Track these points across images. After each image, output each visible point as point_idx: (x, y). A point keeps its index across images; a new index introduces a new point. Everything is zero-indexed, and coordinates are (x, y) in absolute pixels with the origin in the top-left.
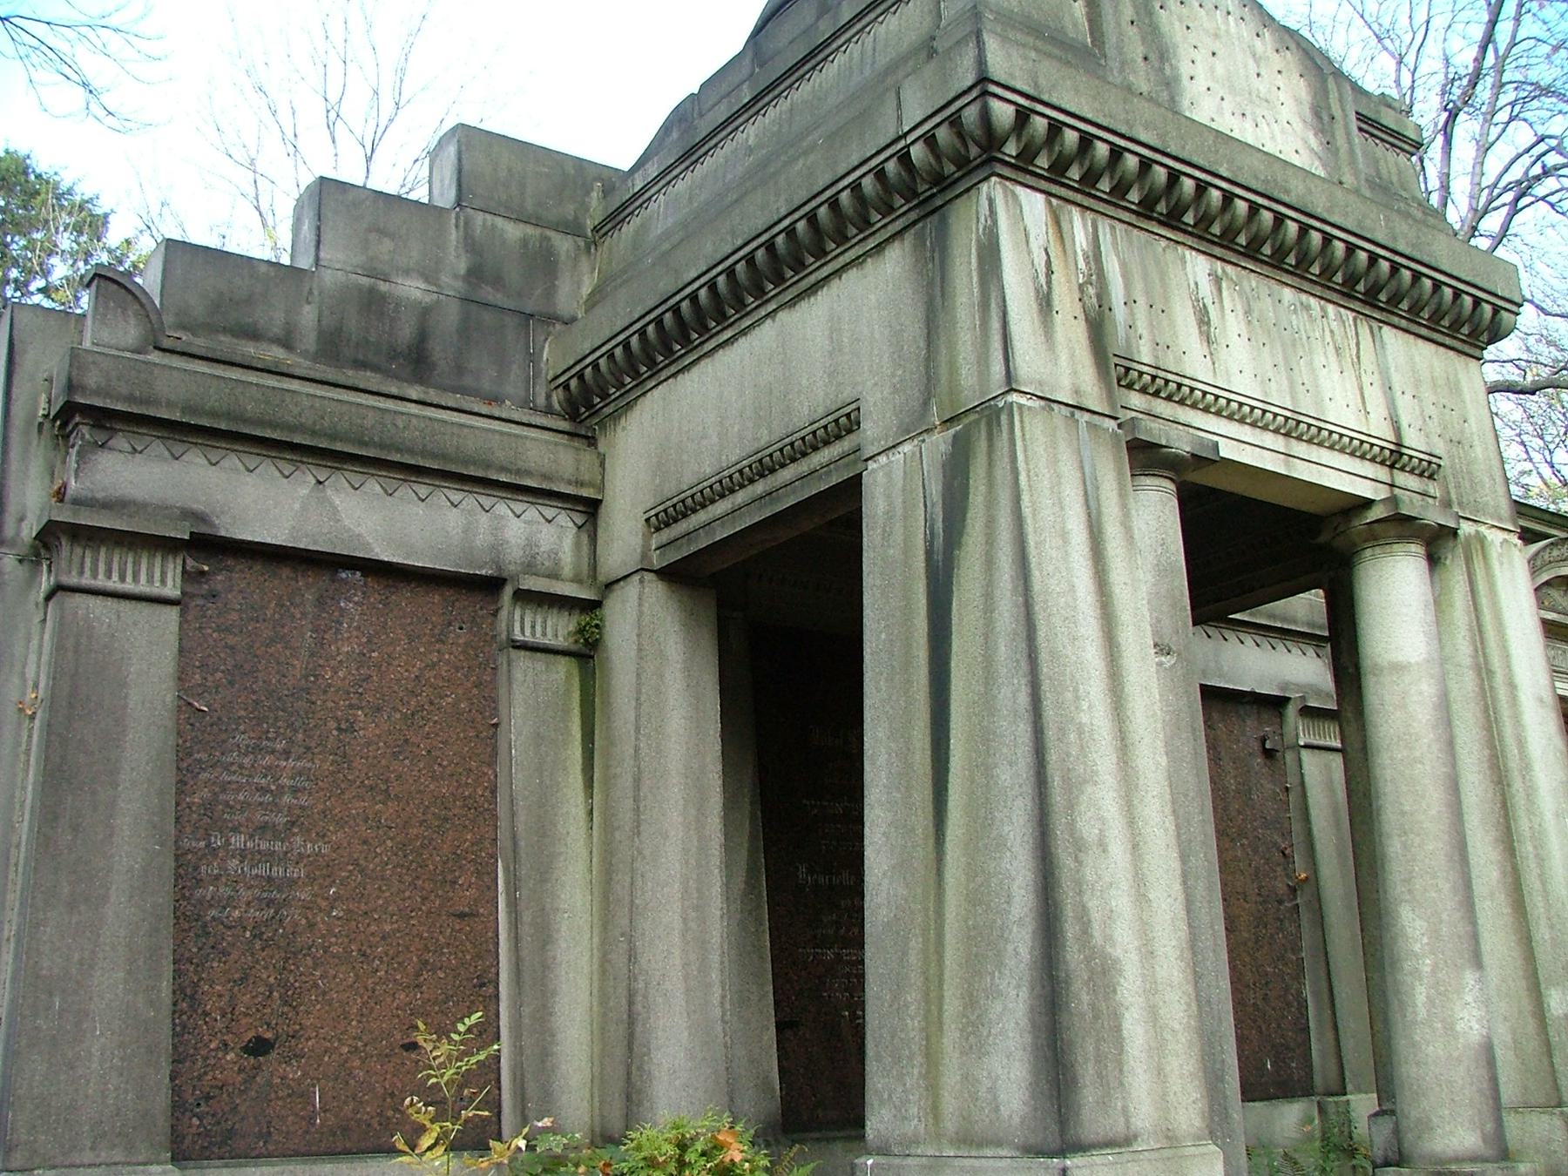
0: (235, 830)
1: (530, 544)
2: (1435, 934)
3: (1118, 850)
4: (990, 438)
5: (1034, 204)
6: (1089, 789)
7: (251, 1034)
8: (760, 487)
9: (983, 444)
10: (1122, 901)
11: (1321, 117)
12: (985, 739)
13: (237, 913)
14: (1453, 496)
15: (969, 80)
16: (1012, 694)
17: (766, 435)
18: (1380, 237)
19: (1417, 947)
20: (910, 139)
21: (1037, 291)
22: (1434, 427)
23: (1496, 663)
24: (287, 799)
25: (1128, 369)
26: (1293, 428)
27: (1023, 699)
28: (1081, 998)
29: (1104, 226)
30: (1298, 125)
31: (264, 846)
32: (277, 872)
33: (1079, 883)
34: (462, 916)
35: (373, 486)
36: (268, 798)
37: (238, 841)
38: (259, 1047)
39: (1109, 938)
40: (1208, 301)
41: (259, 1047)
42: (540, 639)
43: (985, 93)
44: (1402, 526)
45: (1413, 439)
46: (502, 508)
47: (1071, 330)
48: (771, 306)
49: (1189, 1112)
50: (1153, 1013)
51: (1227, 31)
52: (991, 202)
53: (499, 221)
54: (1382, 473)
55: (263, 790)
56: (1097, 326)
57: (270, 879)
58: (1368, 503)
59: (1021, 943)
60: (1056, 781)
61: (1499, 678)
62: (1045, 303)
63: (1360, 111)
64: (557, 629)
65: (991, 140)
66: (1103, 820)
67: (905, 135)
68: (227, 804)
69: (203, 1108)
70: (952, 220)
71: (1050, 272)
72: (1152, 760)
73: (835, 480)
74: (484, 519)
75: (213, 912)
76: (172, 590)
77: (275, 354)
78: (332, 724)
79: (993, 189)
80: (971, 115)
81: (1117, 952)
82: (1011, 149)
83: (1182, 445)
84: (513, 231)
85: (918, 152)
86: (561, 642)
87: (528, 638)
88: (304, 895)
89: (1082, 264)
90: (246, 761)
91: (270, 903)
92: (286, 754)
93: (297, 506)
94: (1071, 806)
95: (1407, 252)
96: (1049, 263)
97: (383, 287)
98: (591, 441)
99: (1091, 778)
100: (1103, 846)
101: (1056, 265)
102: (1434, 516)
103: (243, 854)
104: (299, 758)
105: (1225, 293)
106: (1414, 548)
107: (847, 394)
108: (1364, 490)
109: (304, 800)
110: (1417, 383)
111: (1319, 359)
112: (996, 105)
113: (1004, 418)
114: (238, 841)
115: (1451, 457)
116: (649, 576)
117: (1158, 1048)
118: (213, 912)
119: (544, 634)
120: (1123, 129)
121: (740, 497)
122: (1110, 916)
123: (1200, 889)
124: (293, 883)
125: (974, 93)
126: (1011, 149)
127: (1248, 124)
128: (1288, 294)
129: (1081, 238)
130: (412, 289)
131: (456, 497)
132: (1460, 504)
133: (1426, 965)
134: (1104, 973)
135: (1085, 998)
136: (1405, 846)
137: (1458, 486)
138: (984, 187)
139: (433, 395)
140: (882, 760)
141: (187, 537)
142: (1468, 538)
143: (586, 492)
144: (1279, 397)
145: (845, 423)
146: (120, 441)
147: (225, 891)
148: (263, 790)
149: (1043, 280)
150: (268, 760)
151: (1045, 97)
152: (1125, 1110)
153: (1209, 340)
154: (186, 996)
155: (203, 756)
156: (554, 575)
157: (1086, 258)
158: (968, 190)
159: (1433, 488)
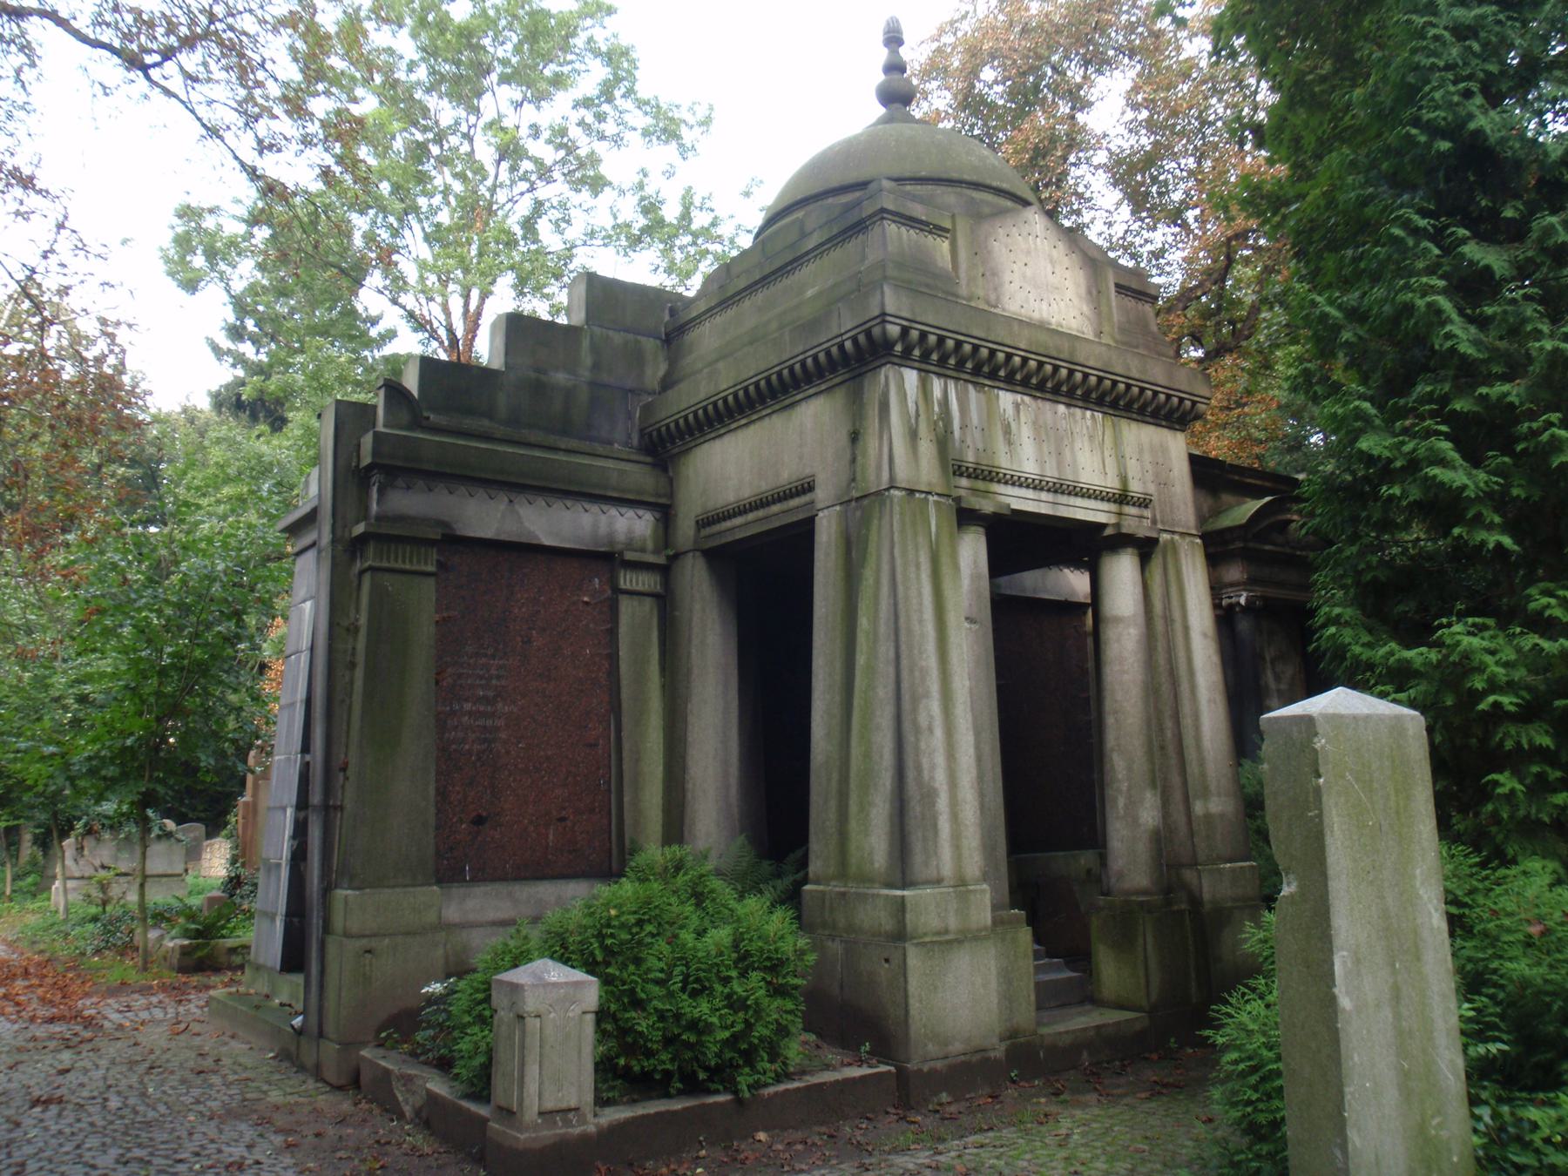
0: (467, 700)
1: (630, 531)
2: (1130, 769)
3: (939, 732)
4: (880, 512)
5: (911, 377)
6: (924, 701)
7: (474, 814)
8: (761, 513)
9: (877, 515)
10: (940, 759)
11: (1095, 293)
12: (871, 670)
13: (467, 747)
14: (1158, 517)
15: (876, 312)
16: (885, 650)
17: (765, 486)
18: (1119, 370)
19: (1120, 776)
20: (845, 337)
21: (910, 428)
22: (1149, 477)
23: (1177, 614)
24: (494, 682)
25: (960, 467)
26: (1058, 488)
27: (892, 654)
28: (915, 808)
29: (951, 385)
30: (1076, 301)
31: (482, 708)
32: (489, 723)
33: (917, 748)
34: (591, 745)
35: (541, 502)
36: (483, 682)
37: (468, 706)
38: (479, 821)
39: (932, 778)
40: (1011, 420)
41: (479, 821)
42: (635, 587)
43: (884, 321)
44: (1121, 541)
45: (1135, 487)
46: (613, 511)
47: (927, 448)
48: (769, 411)
49: (974, 863)
50: (955, 817)
51: (1036, 249)
52: (887, 378)
53: (611, 333)
54: (1113, 507)
55: (481, 678)
56: (943, 442)
57: (485, 727)
58: (1103, 526)
59: (886, 779)
60: (906, 697)
61: (1178, 626)
62: (913, 435)
63: (1122, 282)
64: (645, 581)
65: (888, 344)
66: (932, 717)
67: (841, 335)
68: (461, 686)
69: (449, 855)
70: (866, 384)
71: (918, 415)
72: (962, 684)
73: (801, 516)
74: (603, 518)
75: (454, 747)
76: (431, 568)
77: (485, 424)
78: (519, 639)
79: (887, 373)
80: (876, 331)
81: (937, 785)
82: (898, 348)
83: (987, 507)
84: (618, 338)
85: (848, 345)
86: (646, 588)
87: (628, 586)
88: (503, 735)
89: (936, 408)
90: (472, 661)
91: (485, 740)
92: (493, 657)
93: (499, 515)
94: (915, 710)
95: (1137, 376)
96: (917, 411)
97: (542, 377)
98: (665, 470)
99: (927, 695)
100: (930, 729)
101: (921, 412)
102: (1142, 530)
103: (470, 713)
104: (501, 659)
105: (1022, 414)
106: (1130, 550)
107: (808, 471)
108: (1101, 518)
109: (503, 682)
110: (1141, 451)
111: (1078, 445)
112: (889, 327)
113: (888, 502)
114: (468, 706)
115: (1159, 494)
116: (698, 554)
117: (956, 837)
118: (454, 747)
119: (637, 584)
120: (964, 331)
121: (751, 516)
122: (933, 767)
123: (987, 749)
124: (498, 729)
125: (878, 320)
126: (898, 348)
127: (1044, 306)
128: (1062, 408)
129: (937, 392)
130: (560, 377)
131: (587, 506)
132: (1163, 522)
133: (1124, 786)
134: (930, 796)
135: (918, 809)
136: (1117, 720)
137: (1162, 512)
138: (883, 370)
139: (574, 444)
140: (821, 677)
141: (439, 537)
142: (1166, 542)
143: (662, 501)
144: (1051, 473)
145: (807, 487)
146: (400, 482)
147: (460, 734)
148: (481, 678)
149: (913, 421)
150: (484, 660)
151: (918, 319)
152: (938, 866)
153: (1010, 443)
154: (442, 794)
155: (449, 659)
156: (643, 550)
157: (939, 404)
158: (875, 368)
159: (1147, 513)
